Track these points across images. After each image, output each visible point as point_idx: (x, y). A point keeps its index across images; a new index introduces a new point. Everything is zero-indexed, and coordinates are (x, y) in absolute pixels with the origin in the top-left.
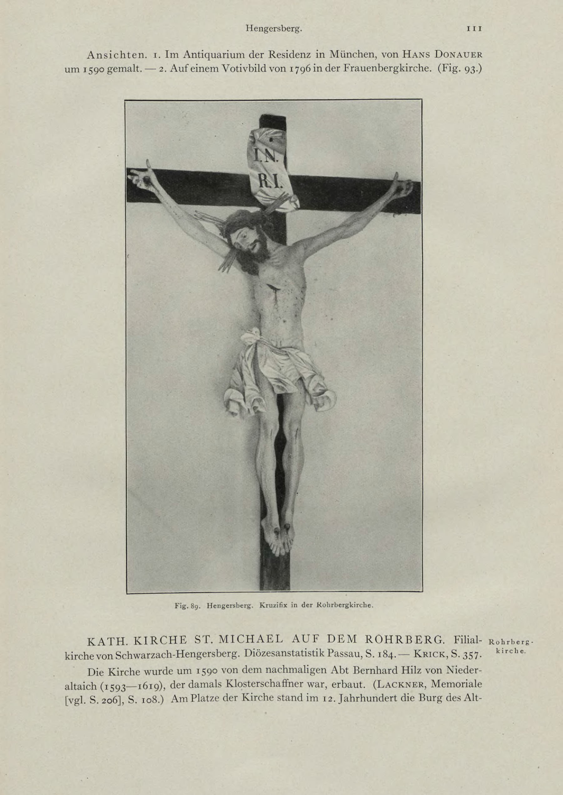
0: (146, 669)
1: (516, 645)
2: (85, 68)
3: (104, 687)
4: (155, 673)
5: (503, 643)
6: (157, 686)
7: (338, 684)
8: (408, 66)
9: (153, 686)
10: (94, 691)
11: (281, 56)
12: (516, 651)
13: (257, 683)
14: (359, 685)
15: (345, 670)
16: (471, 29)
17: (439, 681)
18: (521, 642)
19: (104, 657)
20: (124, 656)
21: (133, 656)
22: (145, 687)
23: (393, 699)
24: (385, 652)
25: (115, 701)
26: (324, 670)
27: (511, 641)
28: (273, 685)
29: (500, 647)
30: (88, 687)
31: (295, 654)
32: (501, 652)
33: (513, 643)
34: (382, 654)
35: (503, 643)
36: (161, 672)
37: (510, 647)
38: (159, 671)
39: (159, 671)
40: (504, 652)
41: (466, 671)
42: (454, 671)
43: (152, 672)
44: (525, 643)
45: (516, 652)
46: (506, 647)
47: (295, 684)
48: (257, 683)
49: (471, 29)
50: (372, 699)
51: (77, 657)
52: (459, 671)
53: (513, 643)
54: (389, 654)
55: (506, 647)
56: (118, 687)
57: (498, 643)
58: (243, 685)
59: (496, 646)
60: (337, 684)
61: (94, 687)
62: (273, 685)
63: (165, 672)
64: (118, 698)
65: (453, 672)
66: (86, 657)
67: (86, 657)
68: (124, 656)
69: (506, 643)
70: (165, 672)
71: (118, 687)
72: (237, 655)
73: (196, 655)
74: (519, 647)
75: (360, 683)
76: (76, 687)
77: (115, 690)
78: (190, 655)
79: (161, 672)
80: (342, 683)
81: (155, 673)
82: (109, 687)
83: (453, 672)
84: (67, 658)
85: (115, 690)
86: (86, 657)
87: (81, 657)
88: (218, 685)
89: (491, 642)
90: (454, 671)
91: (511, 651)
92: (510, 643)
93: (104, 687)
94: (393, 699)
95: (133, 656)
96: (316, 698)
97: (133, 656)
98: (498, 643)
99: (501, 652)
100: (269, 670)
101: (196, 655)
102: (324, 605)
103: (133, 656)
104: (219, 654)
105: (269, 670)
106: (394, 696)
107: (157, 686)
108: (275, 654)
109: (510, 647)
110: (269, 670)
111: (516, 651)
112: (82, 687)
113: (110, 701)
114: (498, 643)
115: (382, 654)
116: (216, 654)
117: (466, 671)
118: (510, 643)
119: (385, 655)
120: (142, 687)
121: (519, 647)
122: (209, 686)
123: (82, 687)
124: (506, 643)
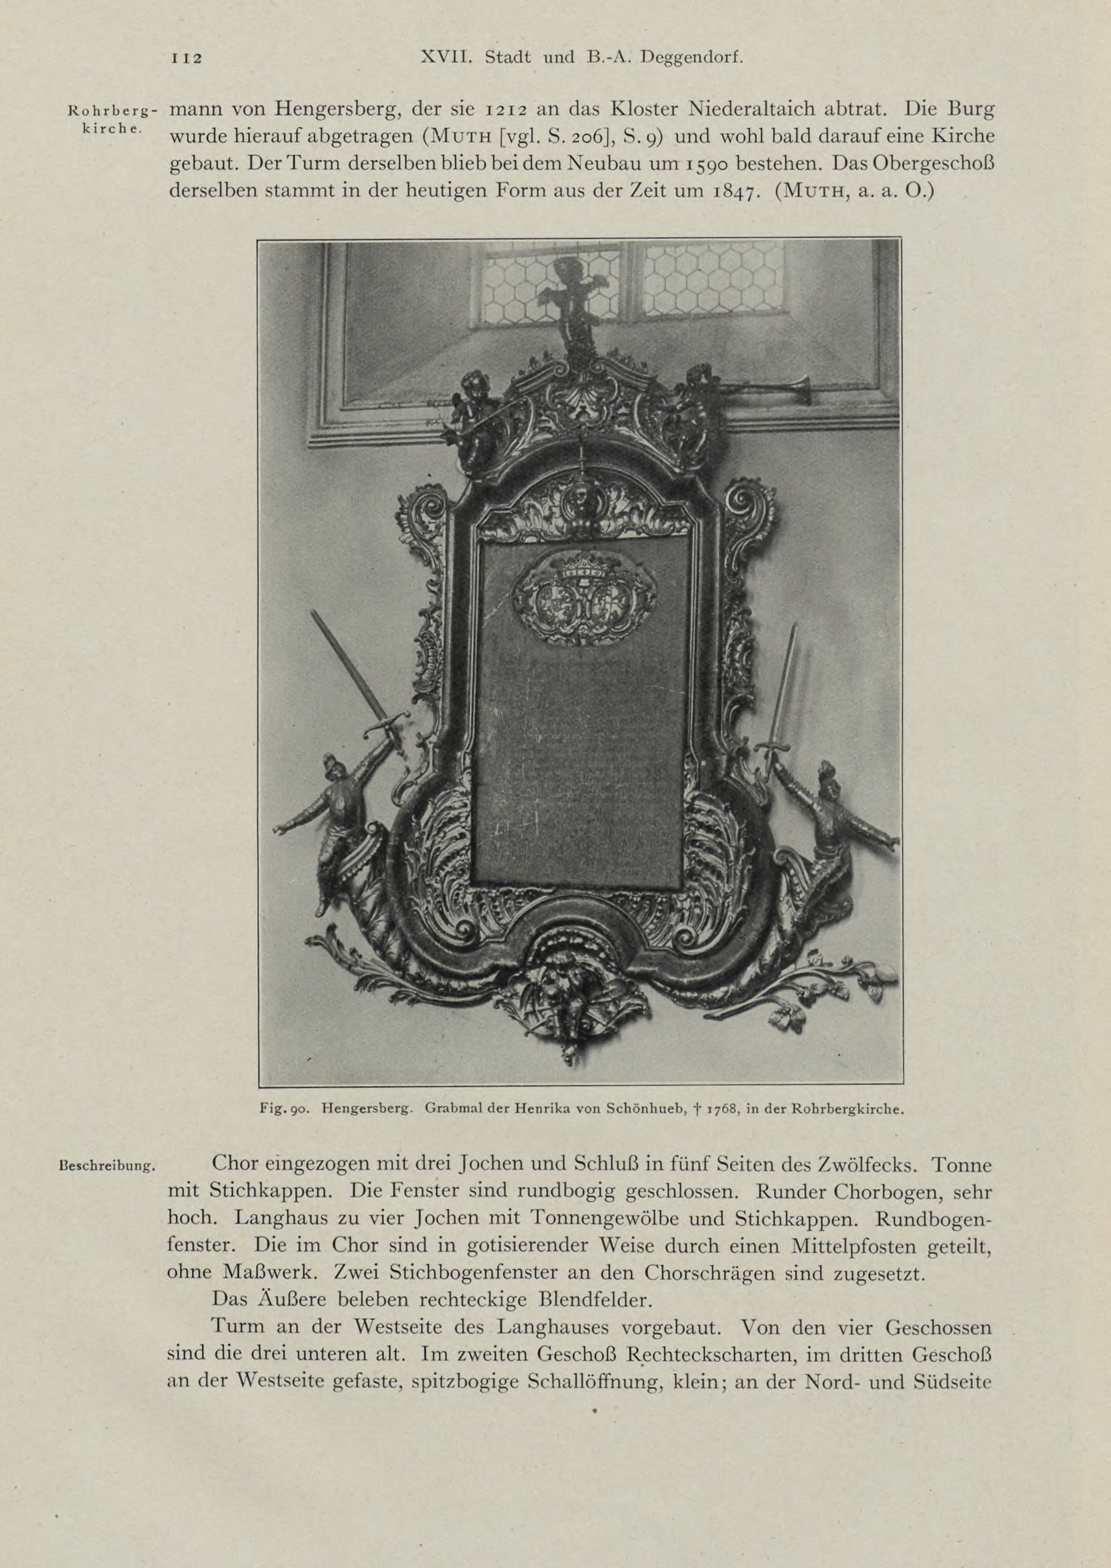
0: (175, 131)
1: (121, 118)
2: (186, 62)
4: (191, 139)
5: (97, 112)
11: (942, 165)
12: (122, 129)
13: (194, 189)
14: (440, 190)
15: (848, 109)
16: (181, 58)
25: (598, 138)
26: (407, 137)
29: (90, 120)
30: (799, 109)
32: (91, 130)
35: (97, 112)
36: (204, 138)
37: (111, 121)
38: (200, 135)
39: (200, 135)
40: (99, 130)
41: (727, 111)
42: (705, 112)
43: (185, 137)
44: (139, 113)
45: (123, 130)
46: (102, 120)
48: (373, 162)
49: (181, 58)
50: (881, 1383)
52: (713, 110)
55: (102, 120)
57: (86, 112)
61: (810, 110)
63: (211, 138)
64: (604, 133)
65: (701, 113)
70: (211, 138)
73: (315, 111)
74: (128, 122)
76: (775, 111)
79: (204, 138)
81: (191, 139)
83: (701, 113)
89: (72, 111)
90: (705, 112)
91: (112, 130)
92: (110, 113)
96: (315, 1246)
98: (86, 113)
99: (91, 130)
102: (807, 1110)
104: (361, 110)
106: (763, 1351)
109: (111, 121)
111: (122, 129)
112: (787, 110)
113: (587, 138)
114: (86, 112)
117: (727, 111)
118: (110, 113)
121: (128, 122)
123: (787, 110)
124: (102, 112)
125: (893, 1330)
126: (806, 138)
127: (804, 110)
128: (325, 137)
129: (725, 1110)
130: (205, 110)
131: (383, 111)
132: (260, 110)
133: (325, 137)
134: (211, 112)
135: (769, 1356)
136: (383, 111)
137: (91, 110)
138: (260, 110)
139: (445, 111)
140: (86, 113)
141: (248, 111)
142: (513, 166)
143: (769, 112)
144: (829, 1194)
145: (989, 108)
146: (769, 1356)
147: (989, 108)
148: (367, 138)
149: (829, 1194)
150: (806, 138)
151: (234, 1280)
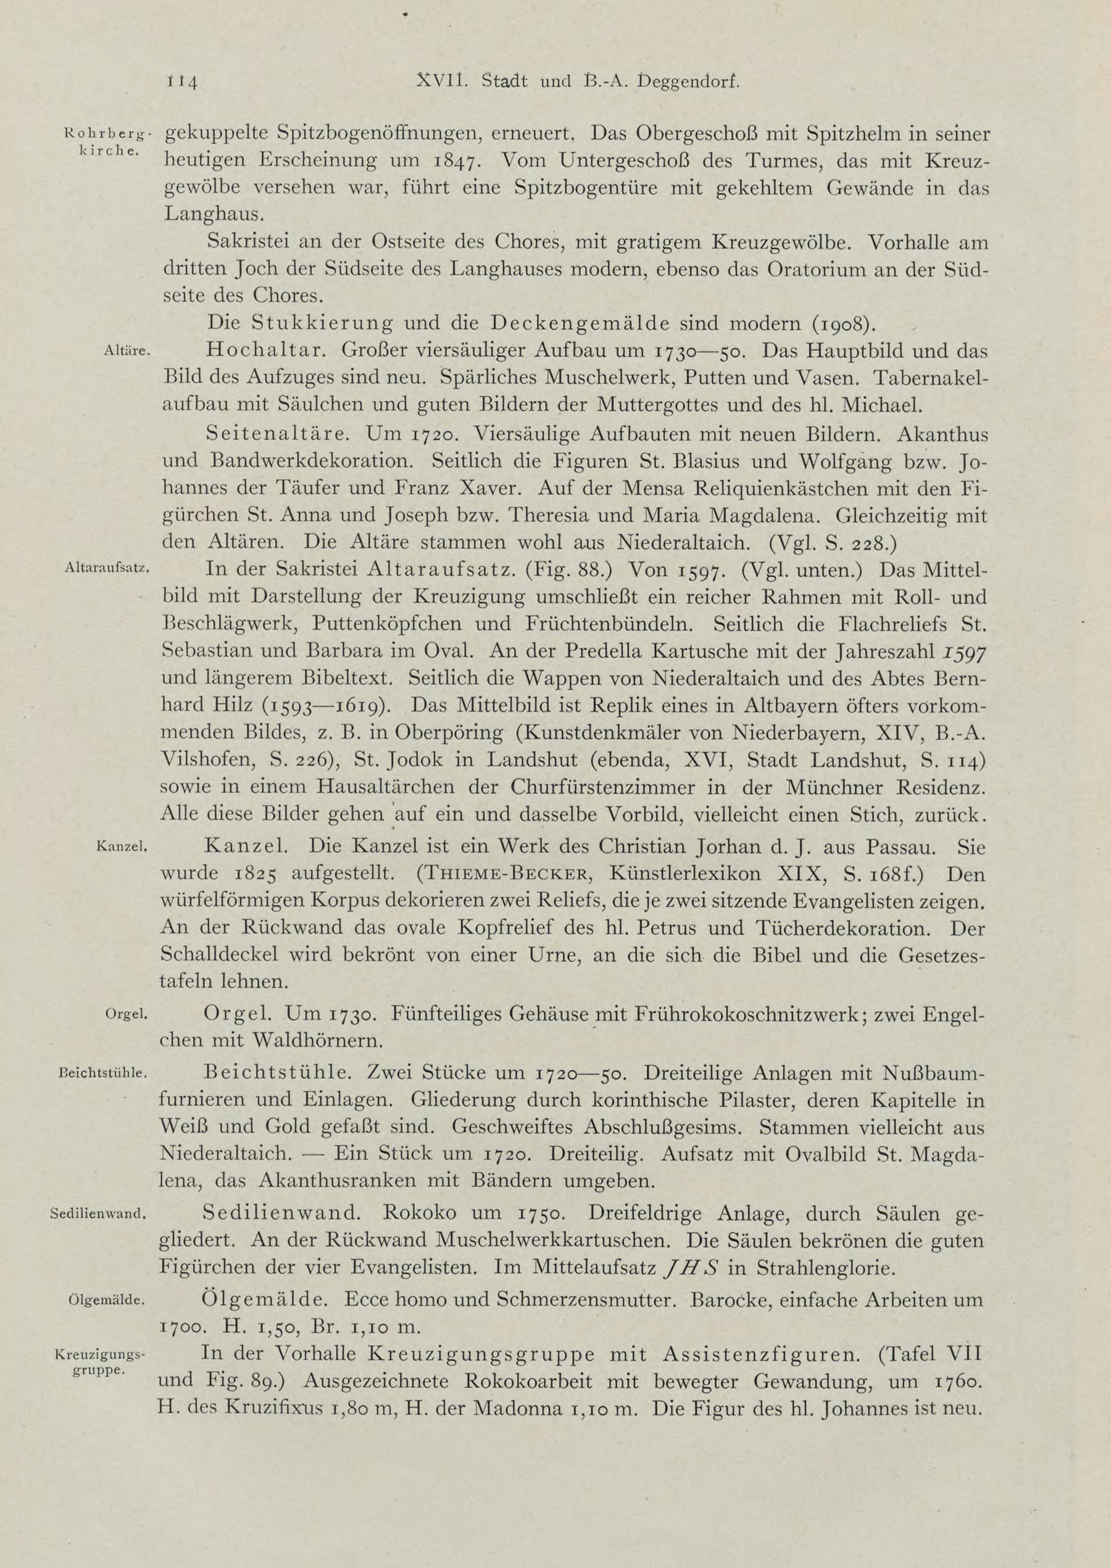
1: (117, 140)
3: (269, 706)
5: (92, 135)
6: (373, 707)
7: (790, 731)
9: (365, 707)
10: (778, 632)
12: (119, 151)
17: (451, 1233)
22: (351, 707)
23: (561, 135)
28: (732, 655)
29: (87, 142)
32: (89, 152)
33: (112, 135)
34: (442, 160)
35: (92, 135)
40: (96, 152)
46: (98, 142)
47: (819, 816)
53: (112, 135)
54: (455, 159)
56: (296, 707)
57: (81, 134)
58: (613, 1129)
60: (788, 733)
62: (732, 655)
71: (296, 707)
75: (897, 758)
77: (699, 577)
80: (891, 1299)
82: (279, 706)
85: (699, 577)
88: (189, 761)
89: (68, 133)
91: (109, 152)
92: (106, 135)
93: (269, 706)
94: (561, 135)
98: (81, 135)
99: (89, 152)
107: (373, 707)
109: (109, 143)
111: (119, 151)
114: (81, 134)
115: (442, 160)
118: (106, 135)
119: (449, 163)
120: (344, 707)
121: (126, 144)
122: (547, 1018)
124: (98, 135)
140: (81, 135)
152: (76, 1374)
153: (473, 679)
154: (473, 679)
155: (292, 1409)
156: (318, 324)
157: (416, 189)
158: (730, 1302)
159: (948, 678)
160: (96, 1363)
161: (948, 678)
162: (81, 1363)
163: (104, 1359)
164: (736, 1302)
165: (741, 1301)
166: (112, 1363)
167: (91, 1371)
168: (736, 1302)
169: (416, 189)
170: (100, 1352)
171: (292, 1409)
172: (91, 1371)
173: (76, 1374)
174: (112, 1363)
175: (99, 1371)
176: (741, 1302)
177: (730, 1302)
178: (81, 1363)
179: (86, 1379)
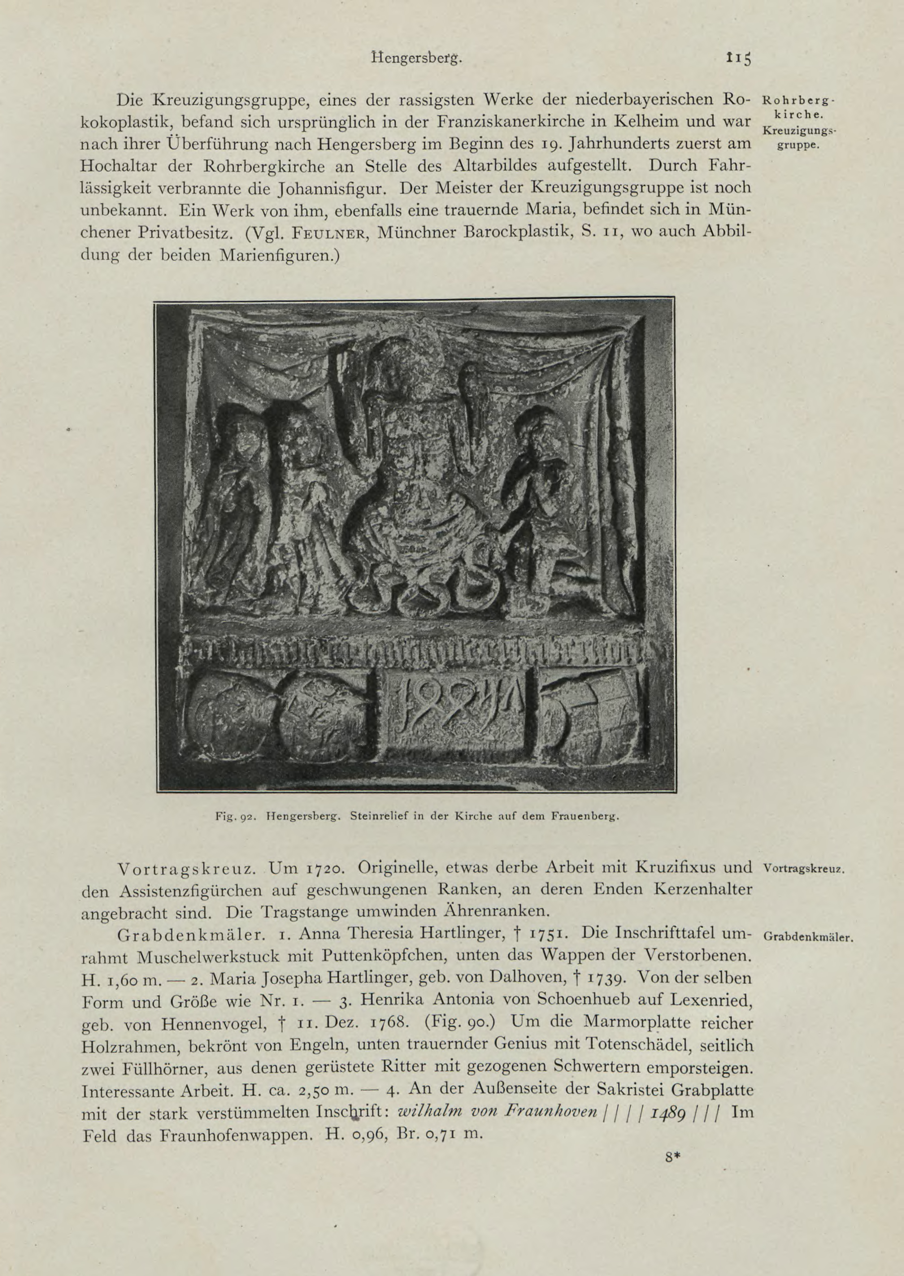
5: (786, 101)
8: (551, 117)
18: (815, 101)
19: (469, 978)
20: (568, 1066)
21: (582, 1067)
24: (400, 1018)
27: (798, 99)
29: (781, 108)
30: (362, 122)
31: (161, 1116)
35: (786, 101)
41: (603, 101)
44: (821, 102)
46: (790, 108)
51: (557, 122)
55: (790, 108)
59: (774, 107)
66: (240, 892)
67: (561, 999)
68: (552, 1000)
69: (791, 101)
72: (456, 1024)
73: (338, 124)
78: (172, 893)
84: (83, 125)
86: (240, 892)
87: (563, 123)
89: (766, 100)
92: (797, 102)
95: (349, 891)
97: (582, 1067)
98: (777, 102)
100: (280, 146)
101: (338, 124)
103: (349, 891)
104: (387, 145)
105: (280, 145)
108: (142, 1093)
110: (280, 146)
116: (382, 145)
117: (603, 101)
118: (797, 102)
124: (791, 101)
125: (500, 1045)
126: (112, 1138)
127: (670, 210)
128: (706, 1092)
129: (391, 1023)
130: (142, 211)
131: (406, 146)
132: (277, 1046)
133: (706, 1092)
134: (324, 192)
135: (614, 1067)
136: (266, 169)
137: (782, 99)
138: (277, 1046)
139: (571, 101)
140: (777, 102)
141: (137, 1027)
142: (659, 1092)
143: (471, 168)
144: (490, 1045)
145: (411, 144)
146: (614, 1067)
147: (411, 144)
148: (419, 1045)
149: (490, 1045)
150: (112, 1138)
151: (219, 986)
152: (780, 148)
153: (307, 145)
154: (307, 145)
155: (690, 869)
156: (546, 122)
157: (217, 146)
158: (496, 233)
159: (460, 143)
160: (797, 139)
161: (460, 143)
162: (784, 138)
163: (803, 135)
164: (501, 233)
165: (504, 232)
166: (809, 139)
167: (793, 146)
168: (501, 233)
169: (217, 146)
170: (800, 129)
171: (690, 869)
172: (793, 146)
173: (780, 148)
174: (809, 139)
175: (799, 146)
176: (505, 233)
177: (496, 233)
178: (784, 138)
179: (789, 152)
